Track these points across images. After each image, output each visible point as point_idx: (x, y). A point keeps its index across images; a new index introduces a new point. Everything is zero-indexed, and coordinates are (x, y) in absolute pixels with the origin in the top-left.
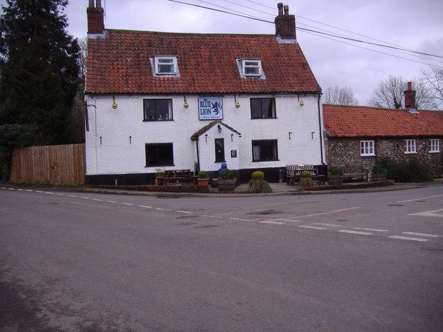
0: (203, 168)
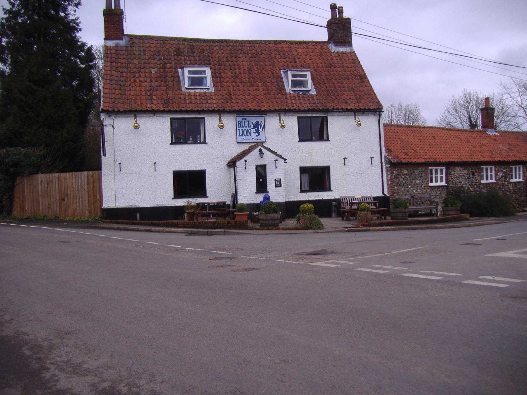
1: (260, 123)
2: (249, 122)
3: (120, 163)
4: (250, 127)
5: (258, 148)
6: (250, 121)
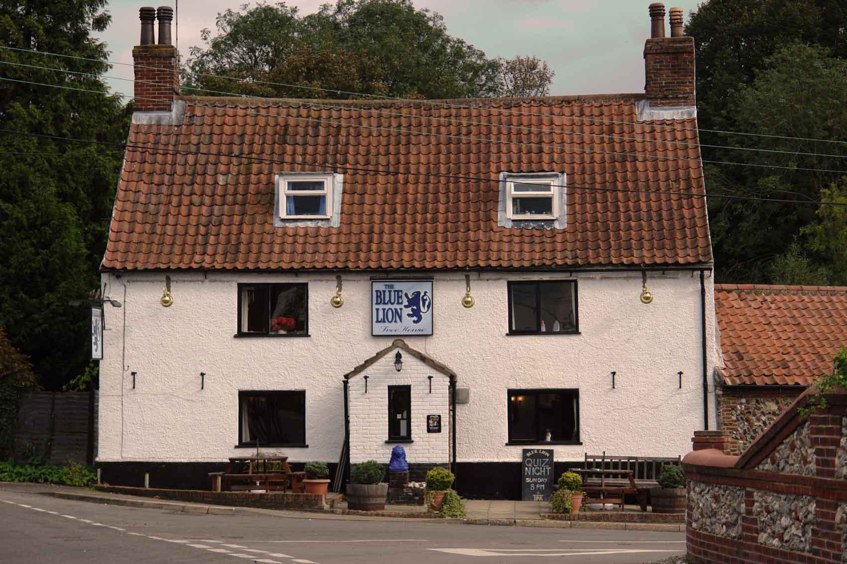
0: (357, 457)
1: (422, 294)
2: (400, 293)
3: (133, 374)
4: (401, 303)
5: (395, 352)
6: (401, 291)
